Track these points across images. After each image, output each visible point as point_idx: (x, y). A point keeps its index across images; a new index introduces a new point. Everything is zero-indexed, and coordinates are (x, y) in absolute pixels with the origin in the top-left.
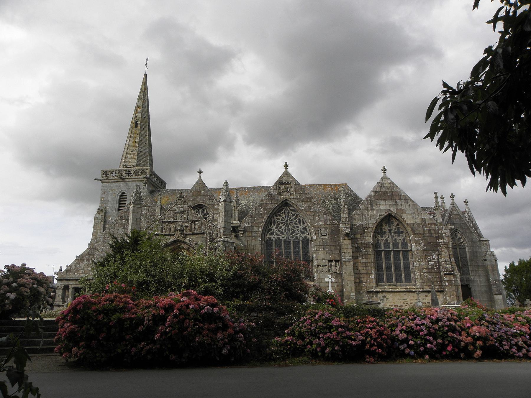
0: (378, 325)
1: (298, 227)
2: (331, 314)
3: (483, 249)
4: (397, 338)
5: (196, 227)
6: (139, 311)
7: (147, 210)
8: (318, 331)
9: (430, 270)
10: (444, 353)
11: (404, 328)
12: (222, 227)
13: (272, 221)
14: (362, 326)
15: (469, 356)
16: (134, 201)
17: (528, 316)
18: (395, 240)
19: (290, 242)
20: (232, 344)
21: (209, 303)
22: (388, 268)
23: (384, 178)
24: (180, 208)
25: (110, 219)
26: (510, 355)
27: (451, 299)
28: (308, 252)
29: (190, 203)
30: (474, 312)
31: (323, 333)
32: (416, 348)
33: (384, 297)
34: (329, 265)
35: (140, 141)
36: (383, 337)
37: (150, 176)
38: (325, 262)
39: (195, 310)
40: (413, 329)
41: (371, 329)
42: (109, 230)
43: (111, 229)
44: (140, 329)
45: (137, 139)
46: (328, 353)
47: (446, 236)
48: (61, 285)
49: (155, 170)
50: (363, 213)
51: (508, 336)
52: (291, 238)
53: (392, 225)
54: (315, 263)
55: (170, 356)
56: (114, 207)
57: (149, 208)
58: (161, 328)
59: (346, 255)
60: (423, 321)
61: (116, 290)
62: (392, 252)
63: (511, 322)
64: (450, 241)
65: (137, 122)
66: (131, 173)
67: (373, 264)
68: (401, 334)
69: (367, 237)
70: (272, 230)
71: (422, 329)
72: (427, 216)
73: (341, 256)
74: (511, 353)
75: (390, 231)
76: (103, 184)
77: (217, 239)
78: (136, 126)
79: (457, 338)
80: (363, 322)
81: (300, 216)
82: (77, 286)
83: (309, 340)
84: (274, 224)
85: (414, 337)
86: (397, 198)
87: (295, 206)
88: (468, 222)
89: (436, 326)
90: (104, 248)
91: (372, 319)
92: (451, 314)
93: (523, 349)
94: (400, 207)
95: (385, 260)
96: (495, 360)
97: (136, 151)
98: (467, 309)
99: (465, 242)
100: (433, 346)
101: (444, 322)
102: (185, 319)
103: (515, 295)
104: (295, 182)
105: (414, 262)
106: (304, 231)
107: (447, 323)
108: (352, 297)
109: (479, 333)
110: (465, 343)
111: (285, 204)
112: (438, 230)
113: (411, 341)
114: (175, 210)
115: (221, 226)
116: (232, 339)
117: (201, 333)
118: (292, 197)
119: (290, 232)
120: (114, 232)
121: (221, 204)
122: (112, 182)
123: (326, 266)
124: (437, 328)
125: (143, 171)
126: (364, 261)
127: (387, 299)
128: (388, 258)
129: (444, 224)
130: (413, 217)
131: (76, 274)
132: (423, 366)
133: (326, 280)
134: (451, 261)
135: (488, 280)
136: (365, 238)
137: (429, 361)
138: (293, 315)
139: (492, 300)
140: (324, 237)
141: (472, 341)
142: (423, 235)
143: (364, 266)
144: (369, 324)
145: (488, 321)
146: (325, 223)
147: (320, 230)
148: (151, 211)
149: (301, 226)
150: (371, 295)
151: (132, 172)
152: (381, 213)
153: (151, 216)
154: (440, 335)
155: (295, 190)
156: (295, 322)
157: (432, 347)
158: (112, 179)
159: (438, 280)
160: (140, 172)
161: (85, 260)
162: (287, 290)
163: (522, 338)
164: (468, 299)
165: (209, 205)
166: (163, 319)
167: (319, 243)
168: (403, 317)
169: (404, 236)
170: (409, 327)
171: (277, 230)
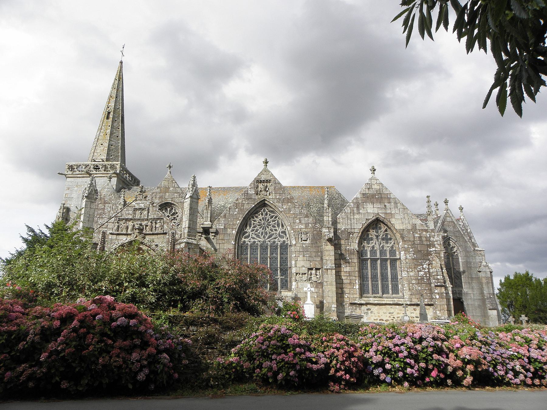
0: (348, 344)
1: (276, 230)
2: (289, 330)
3: (478, 259)
4: (370, 360)
5: (157, 226)
6: (26, 322)
7: (110, 207)
8: (271, 351)
9: (420, 281)
10: (427, 380)
11: (380, 348)
12: (186, 227)
13: (248, 223)
14: (328, 346)
15: (457, 383)
16: (87, 195)
17: (527, 335)
19: (267, 247)
20: (153, 367)
21: (125, 312)
22: (374, 278)
24: (140, 205)
26: (505, 381)
27: (441, 314)
28: (286, 258)
29: (157, 200)
30: (465, 330)
31: (276, 353)
32: (393, 373)
33: (368, 310)
34: (309, 273)
35: (111, 134)
36: (353, 359)
37: (120, 172)
38: (304, 270)
39: (104, 323)
40: (390, 350)
41: (338, 349)
44: (20, 346)
45: (109, 131)
46: (281, 380)
47: (438, 244)
49: (128, 166)
51: (504, 359)
52: (268, 243)
53: (380, 231)
54: (294, 270)
55: (62, 382)
56: (79, 204)
57: (113, 206)
58: (51, 346)
59: (328, 262)
60: (403, 340)
61: (8, 294)
62: (379, 260)
63: (507, 342)
64: (442, 250)
65: (109, 113)
66: (99, 168)
67: (357, 273)
68: (376, 355)
69: (352, 244)
70: (247, 232)
71: (401, 350)
73: (322, 264)
74: (507, 380)
76: (68, 178)
77: (180, 240)
78: (108, 118)
79: (443, 362)
80: (330, 340)
81: (279, 218)
83: (260, 362)
84: (250, 227)
85: (392, 359)
86: (386, 201)
87: (273, 207)
88: (463, 230)
89: (419, 347)
91: (340, 336)
92: (438, 332)
93: (521, 374)
94: (389, 211)
95: (371, 269)
96: (487, 388)
97: (106, 145)
98: (457, 325)
99: (458, 252)
100: (414, 371)
101: (428, 342)
102: (88, 333)
103: (509, 310)
105: (403, 272)
107: (432, 343)
108: (333, 309)
109: (470, 355)
110: (452, 367)
111: (263, 204)
112: (430, 237)
113: (387, 365)
114: (135, 207)
115: (185, 225)
116: (153, 360)
117: (109, 352)
118: (270, 197)
119: (267, 235)
121: (186, 200)
122: (78, 177)
123: (305, 274)
124: (420, 348)
125: (113, 167)
126: (348, 269)
127: (372, 312)
128: (374, 267)
129: (437, 231)
132: (400, 397)
133: (305, 289)
134: (442, 271)
135: (482, 293)
136: (349, 244)
137: (409, 390)
138: (243, 330)
139: (485, 316)
141: (462, 365)
142: (413, 243)
143: (348, 275)
144: (335, 343)
145: (481, 341)
146: (306, 226)
147: (300, 235)
149: (280, 230)
150: (354, 308)
151: (100, 167)
152: (368, 216)
154: (423, 358)
155: (275, 189)
156: (245, 339)
158: (78, 174)
159: (428, 293)
160: (109, 167)
162: (237, 299)
163: (520, 362)
164: (459, 314)
165: (178, 203)
166: (57, 332)
167: (298, 248)
168: (380, 335)
169: (393, 243)
170: (386, 347)
171: (253, 234)
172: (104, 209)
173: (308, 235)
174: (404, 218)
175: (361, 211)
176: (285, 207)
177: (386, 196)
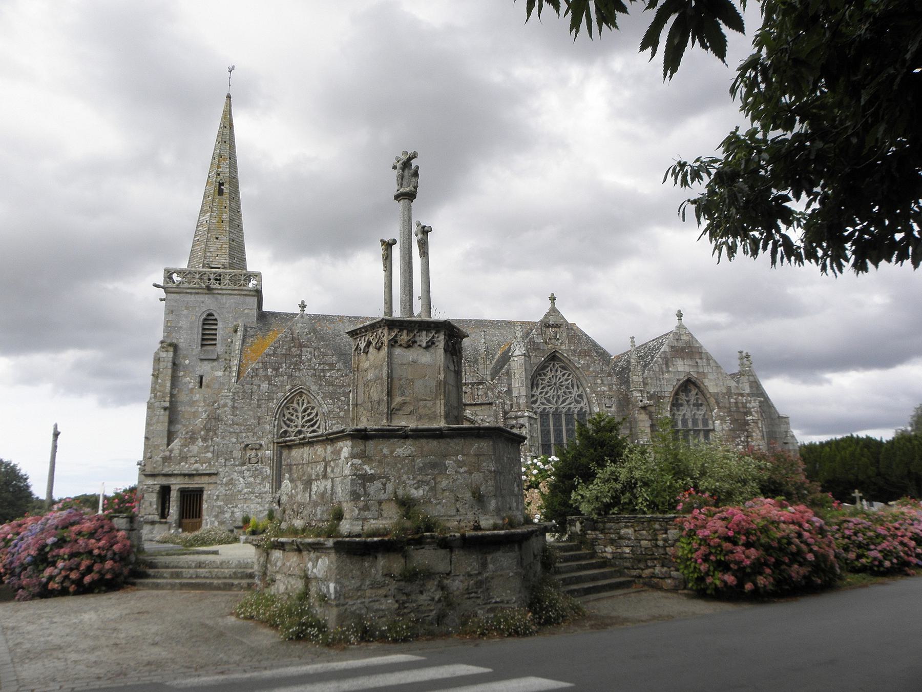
7: (311, 353)
18: (694, 415)
19: (560, 415)
23: (680, 327)
25: (187, 362)
42: (243, 386)
43: (247, 384)
48: (154, 485)
50: (658, 375)
65: (221, 184)
72: (733, 384)
75: (688, 401)
76: (169, 295)
78: (221, 192)
82: (187, 486)
86: (697, 356)
90: (236, 419)
94: (701, 370)
104: (567, 326)
106: (578, 399)
111: (553, 357)
112: (746, 403)
115: (519, 393)
118: (563, 347)
120: (251, 389)
122: (187, 293)
130: (717, 385)
131: (183, 464)
136: (660, 411)
140: (609, 409)
146: (609, 388)
148: (319, 356)
149: (575, 392)
153: (320, 364)
157: (130, 569)
158: (188, 288)
161: (200, 440)
172: (300, 356)
173: (613, 399)
174: (718, 378)
175: (670, 369)
176: (582, 362)
177: (697, 351)
